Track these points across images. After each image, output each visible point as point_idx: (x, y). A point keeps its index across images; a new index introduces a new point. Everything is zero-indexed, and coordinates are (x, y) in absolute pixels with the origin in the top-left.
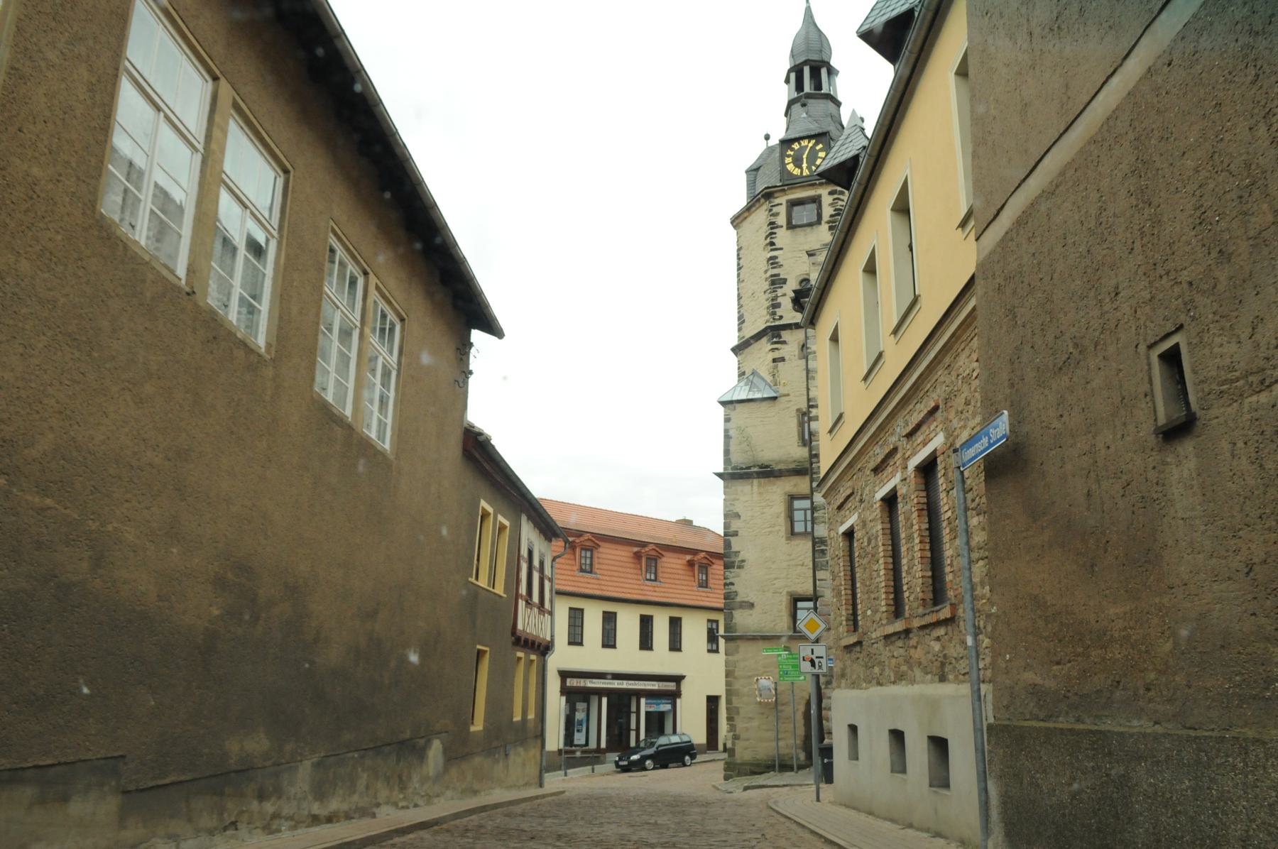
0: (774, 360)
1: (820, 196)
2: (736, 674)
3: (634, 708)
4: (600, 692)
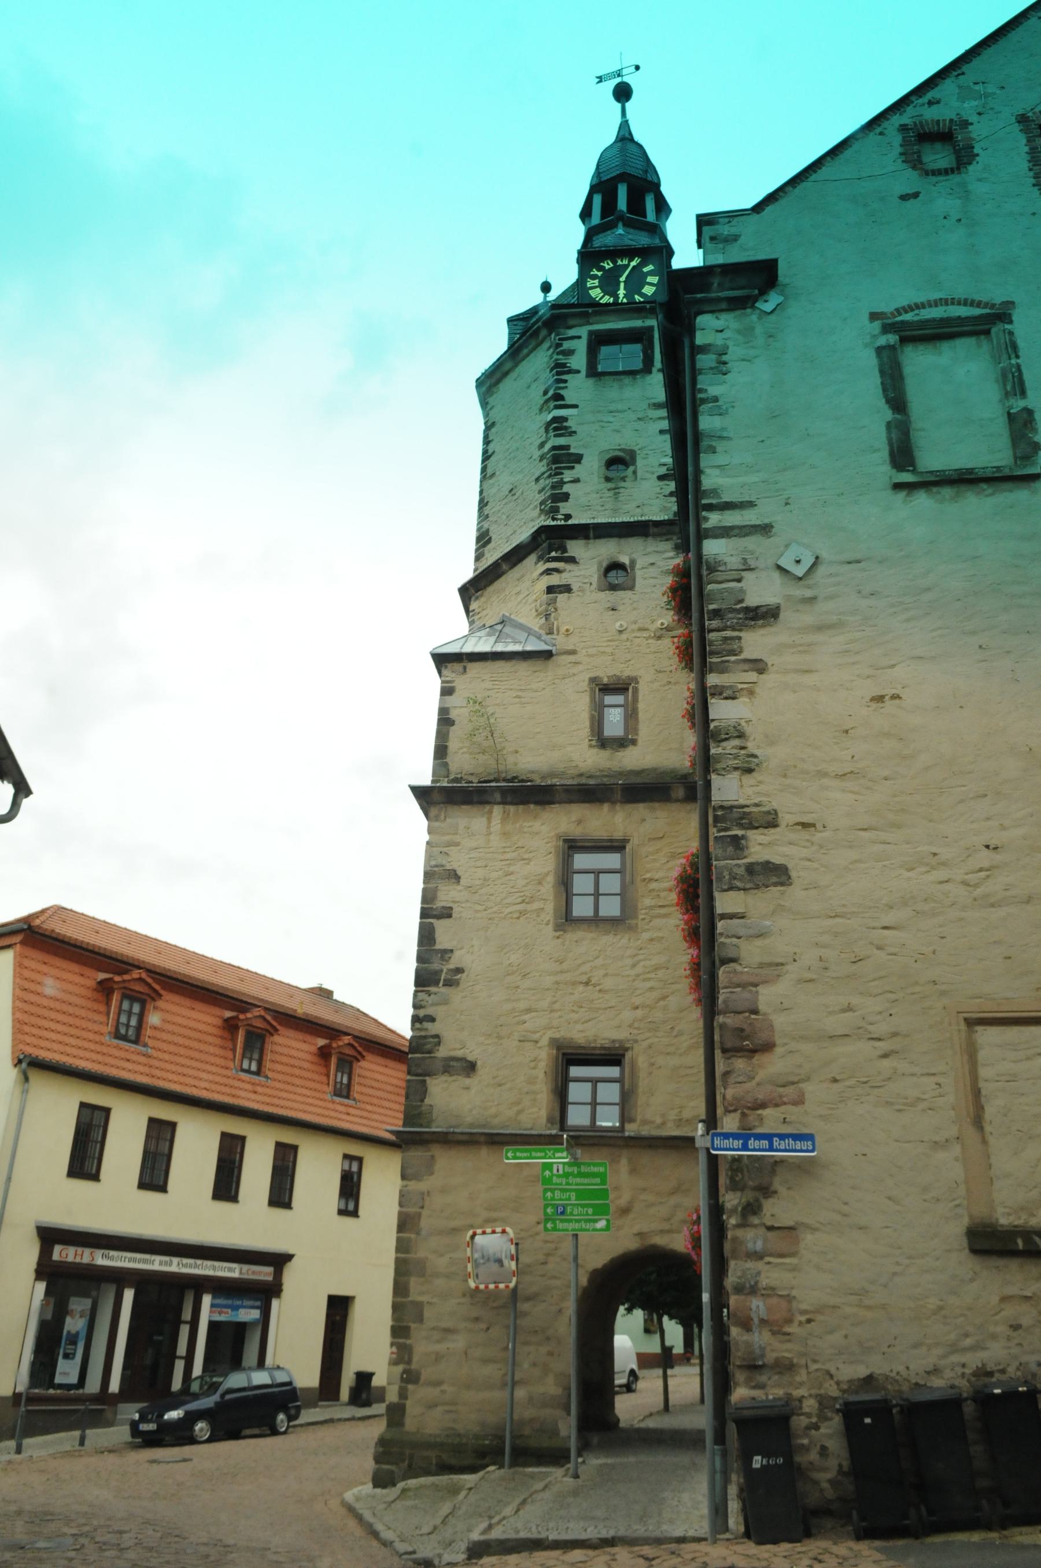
0: (550, 590)
3: (187, 1315)
4: (120, 1278)
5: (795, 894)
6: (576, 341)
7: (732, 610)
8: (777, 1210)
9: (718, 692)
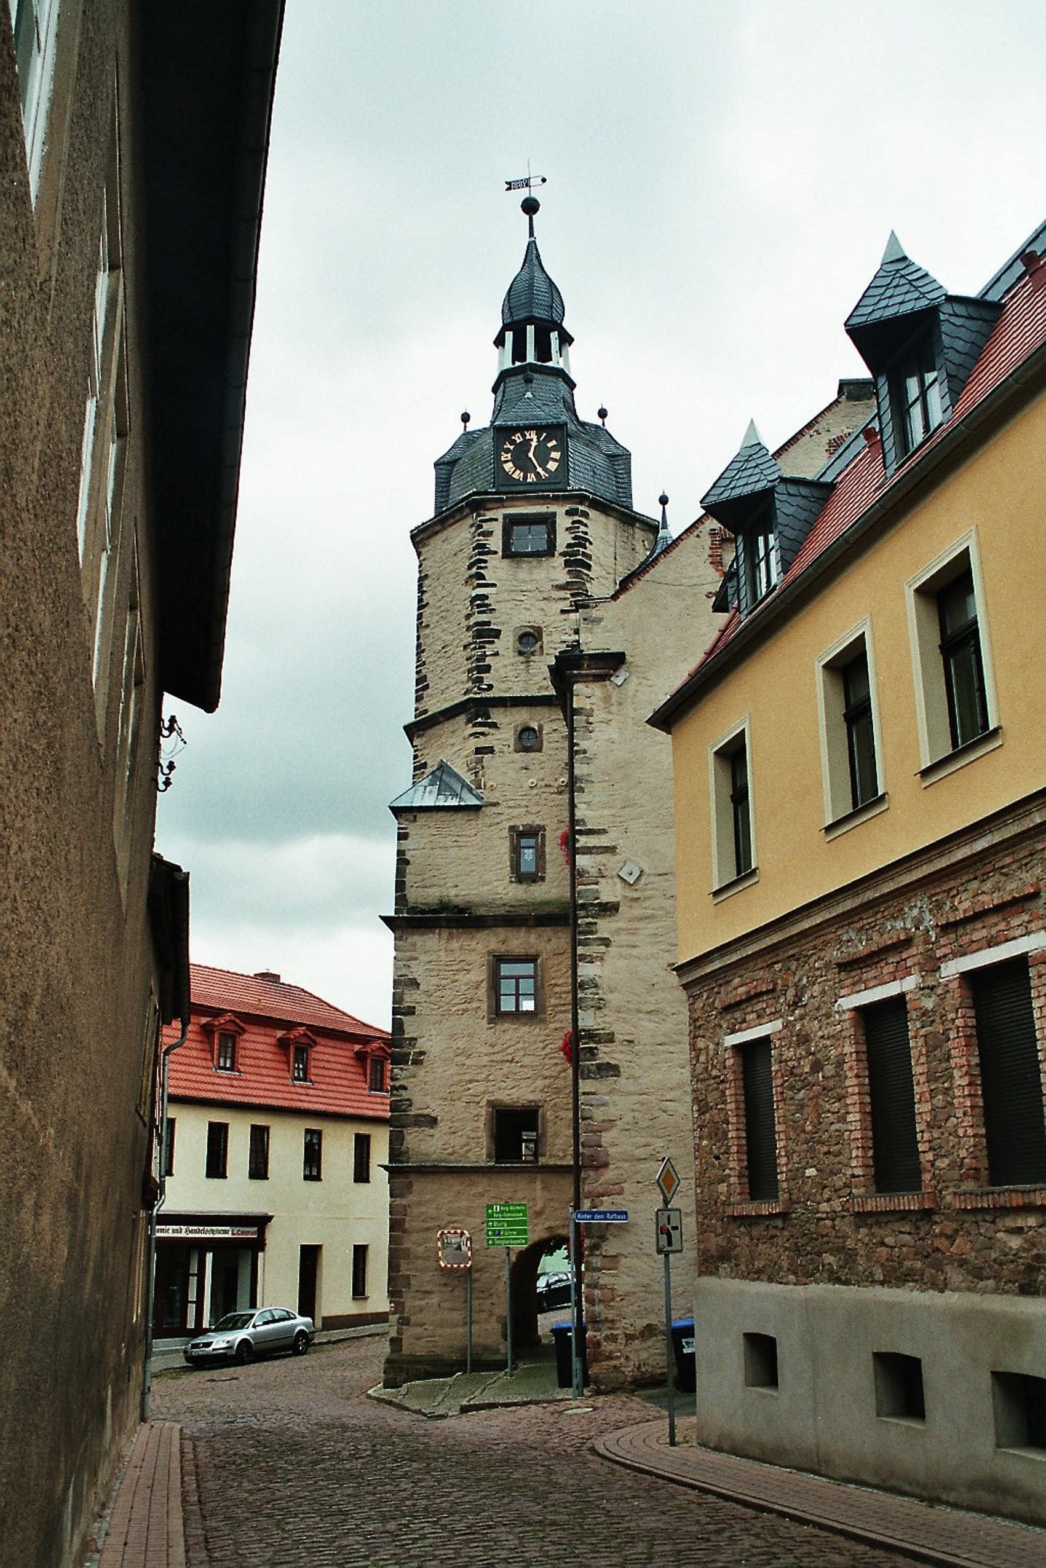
1: (554, 514)
2: (407, 1226)
5: (622, 1082)
6: (494, 523)
7: (592, 905)
8: (611, 1247)
9: (583, 957)
